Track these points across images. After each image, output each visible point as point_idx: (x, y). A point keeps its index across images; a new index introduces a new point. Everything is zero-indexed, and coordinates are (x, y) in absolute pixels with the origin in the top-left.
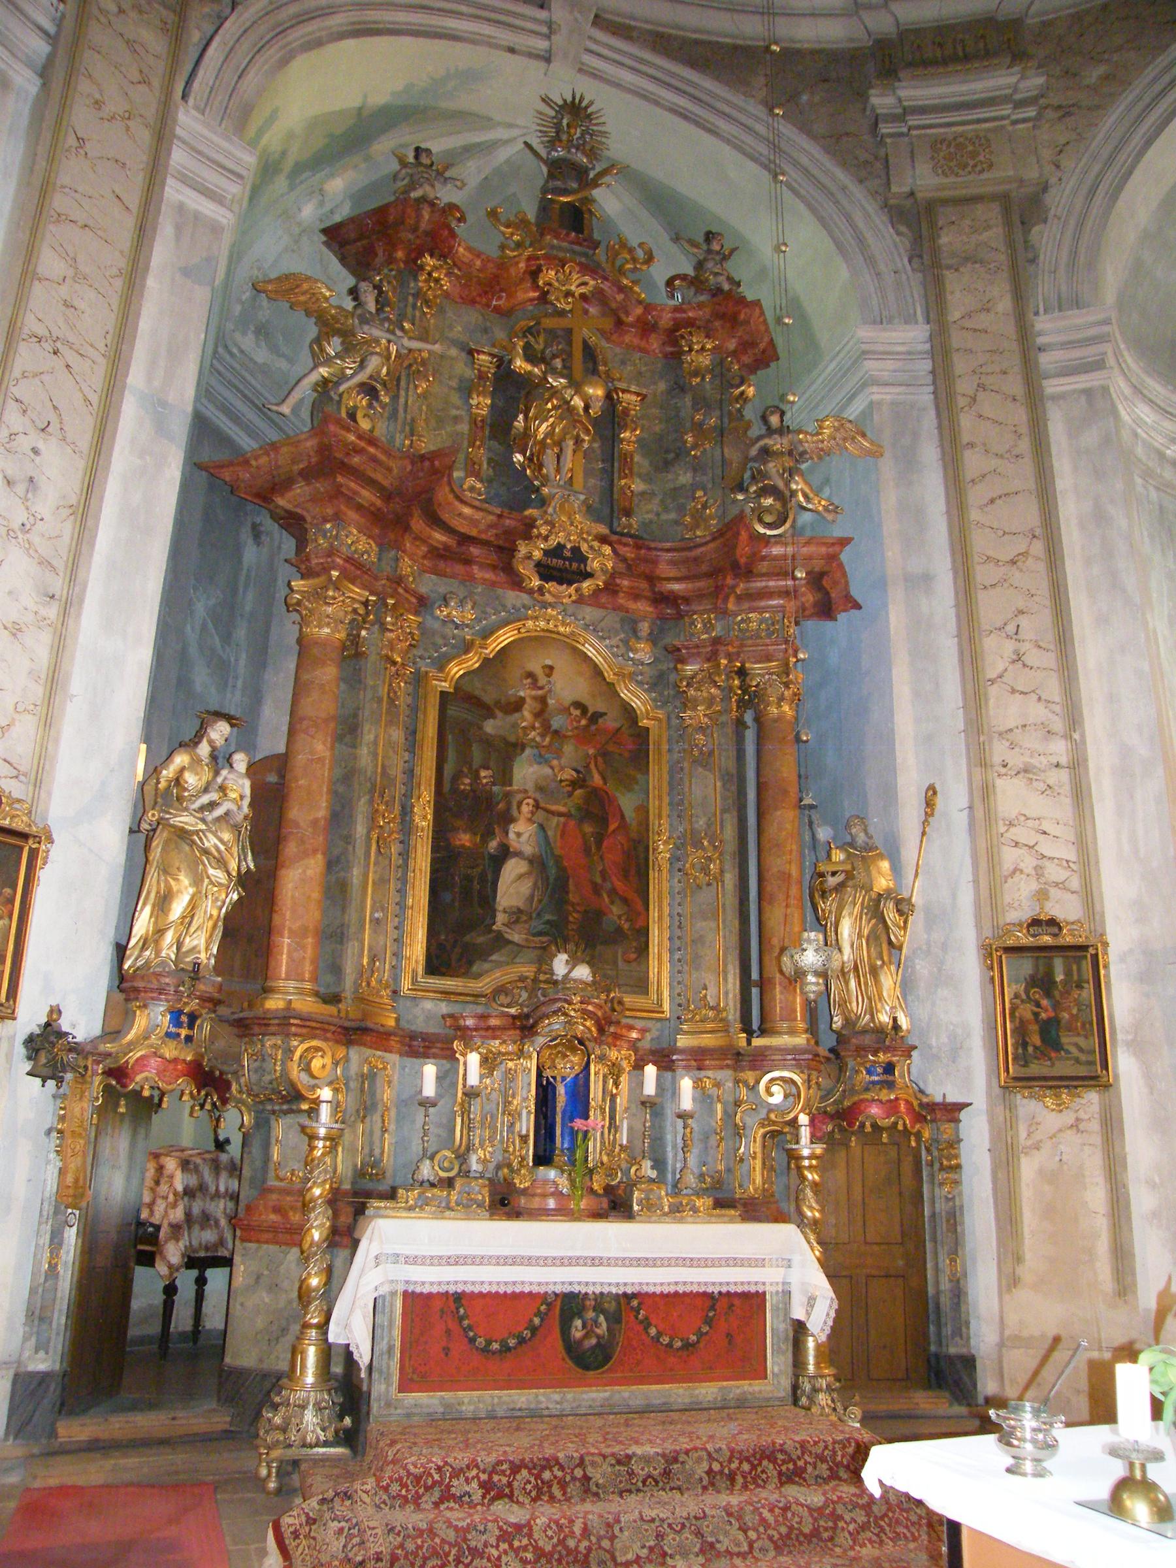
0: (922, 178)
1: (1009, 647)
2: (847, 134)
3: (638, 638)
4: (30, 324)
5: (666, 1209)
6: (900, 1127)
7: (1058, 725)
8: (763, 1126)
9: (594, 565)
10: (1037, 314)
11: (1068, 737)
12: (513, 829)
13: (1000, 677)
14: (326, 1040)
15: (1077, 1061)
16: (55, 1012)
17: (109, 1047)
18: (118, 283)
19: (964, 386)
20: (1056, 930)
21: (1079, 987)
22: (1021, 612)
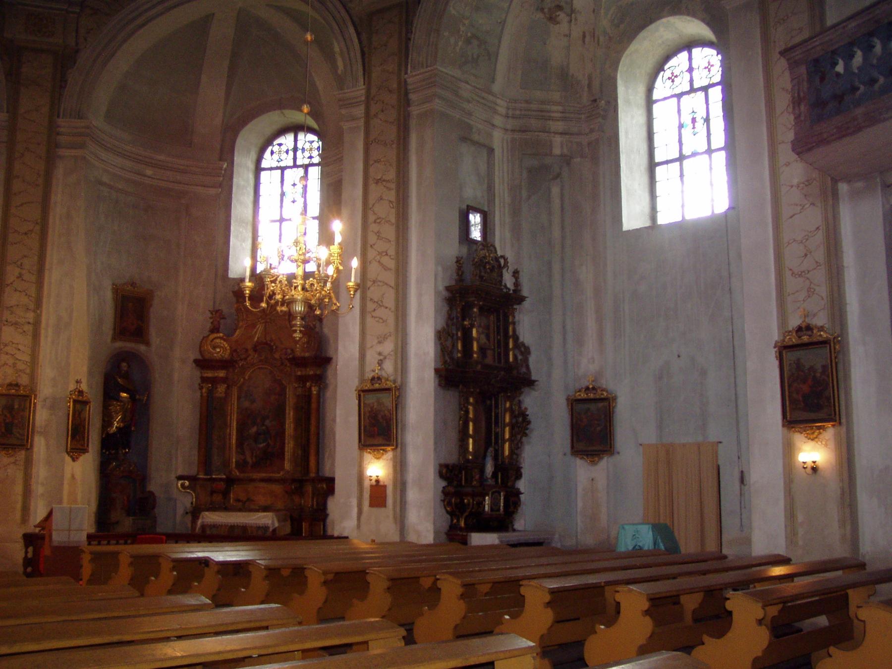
1: (17, 271)
7: (32, 306)
10: (58, 117)
11: (34, 311)
22: (25, 256)
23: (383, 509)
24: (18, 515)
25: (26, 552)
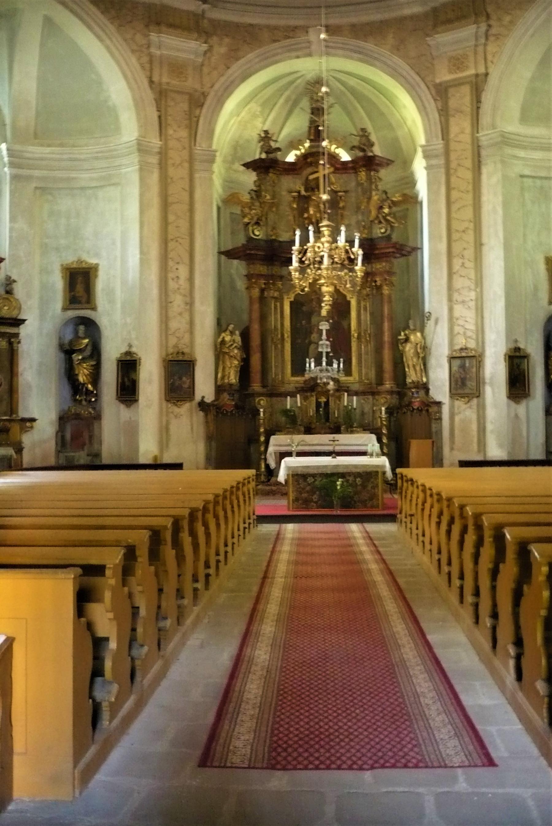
0: (444, 76)
1: (461, 261)
4: (170, 237)
7: (473, 287)
11: (475, 291)
12: (313, 336)
16: (203, 397)
18: (188, 214)
19: (453, 165)
22: (465, 249)
23: (100, 267)
24: (475, 446)
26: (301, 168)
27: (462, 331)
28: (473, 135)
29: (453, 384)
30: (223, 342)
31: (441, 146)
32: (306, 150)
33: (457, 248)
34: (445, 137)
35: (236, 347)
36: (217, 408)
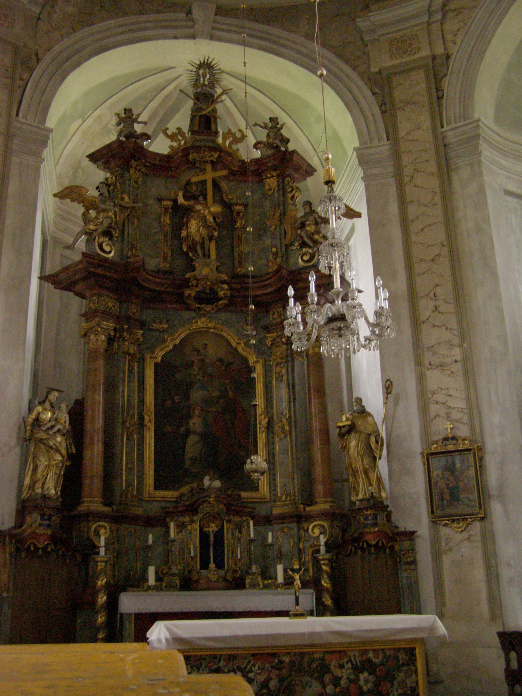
2: (349, 43)
3: (248, 325)
5: (261, 586)
6: (380, 544)
7: (456, 340)
8: (312, 547)
9: (221, 294)
11: (461, 346)
13: (427, 320)
14: (107, 522)
15: (467, 505)
17: (17, 531)
19: (408, 171)
20: (455, 442)
21: (468, 469)
22: (437, 285)
24: (485, 608)
25: (508, 661)
26: (178, 168)
27: (443, 411)
28: (434, 130)
29: (436, 498)
30: (37, 422)
31: (388, 147)
32: (186, 143)
33: (423, 285)
34: (391, 136)
35: (59, 430)
36: (17, 541)
